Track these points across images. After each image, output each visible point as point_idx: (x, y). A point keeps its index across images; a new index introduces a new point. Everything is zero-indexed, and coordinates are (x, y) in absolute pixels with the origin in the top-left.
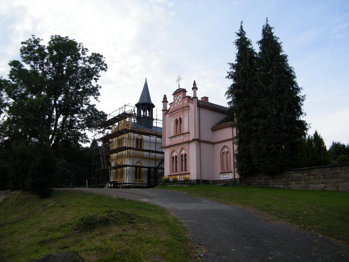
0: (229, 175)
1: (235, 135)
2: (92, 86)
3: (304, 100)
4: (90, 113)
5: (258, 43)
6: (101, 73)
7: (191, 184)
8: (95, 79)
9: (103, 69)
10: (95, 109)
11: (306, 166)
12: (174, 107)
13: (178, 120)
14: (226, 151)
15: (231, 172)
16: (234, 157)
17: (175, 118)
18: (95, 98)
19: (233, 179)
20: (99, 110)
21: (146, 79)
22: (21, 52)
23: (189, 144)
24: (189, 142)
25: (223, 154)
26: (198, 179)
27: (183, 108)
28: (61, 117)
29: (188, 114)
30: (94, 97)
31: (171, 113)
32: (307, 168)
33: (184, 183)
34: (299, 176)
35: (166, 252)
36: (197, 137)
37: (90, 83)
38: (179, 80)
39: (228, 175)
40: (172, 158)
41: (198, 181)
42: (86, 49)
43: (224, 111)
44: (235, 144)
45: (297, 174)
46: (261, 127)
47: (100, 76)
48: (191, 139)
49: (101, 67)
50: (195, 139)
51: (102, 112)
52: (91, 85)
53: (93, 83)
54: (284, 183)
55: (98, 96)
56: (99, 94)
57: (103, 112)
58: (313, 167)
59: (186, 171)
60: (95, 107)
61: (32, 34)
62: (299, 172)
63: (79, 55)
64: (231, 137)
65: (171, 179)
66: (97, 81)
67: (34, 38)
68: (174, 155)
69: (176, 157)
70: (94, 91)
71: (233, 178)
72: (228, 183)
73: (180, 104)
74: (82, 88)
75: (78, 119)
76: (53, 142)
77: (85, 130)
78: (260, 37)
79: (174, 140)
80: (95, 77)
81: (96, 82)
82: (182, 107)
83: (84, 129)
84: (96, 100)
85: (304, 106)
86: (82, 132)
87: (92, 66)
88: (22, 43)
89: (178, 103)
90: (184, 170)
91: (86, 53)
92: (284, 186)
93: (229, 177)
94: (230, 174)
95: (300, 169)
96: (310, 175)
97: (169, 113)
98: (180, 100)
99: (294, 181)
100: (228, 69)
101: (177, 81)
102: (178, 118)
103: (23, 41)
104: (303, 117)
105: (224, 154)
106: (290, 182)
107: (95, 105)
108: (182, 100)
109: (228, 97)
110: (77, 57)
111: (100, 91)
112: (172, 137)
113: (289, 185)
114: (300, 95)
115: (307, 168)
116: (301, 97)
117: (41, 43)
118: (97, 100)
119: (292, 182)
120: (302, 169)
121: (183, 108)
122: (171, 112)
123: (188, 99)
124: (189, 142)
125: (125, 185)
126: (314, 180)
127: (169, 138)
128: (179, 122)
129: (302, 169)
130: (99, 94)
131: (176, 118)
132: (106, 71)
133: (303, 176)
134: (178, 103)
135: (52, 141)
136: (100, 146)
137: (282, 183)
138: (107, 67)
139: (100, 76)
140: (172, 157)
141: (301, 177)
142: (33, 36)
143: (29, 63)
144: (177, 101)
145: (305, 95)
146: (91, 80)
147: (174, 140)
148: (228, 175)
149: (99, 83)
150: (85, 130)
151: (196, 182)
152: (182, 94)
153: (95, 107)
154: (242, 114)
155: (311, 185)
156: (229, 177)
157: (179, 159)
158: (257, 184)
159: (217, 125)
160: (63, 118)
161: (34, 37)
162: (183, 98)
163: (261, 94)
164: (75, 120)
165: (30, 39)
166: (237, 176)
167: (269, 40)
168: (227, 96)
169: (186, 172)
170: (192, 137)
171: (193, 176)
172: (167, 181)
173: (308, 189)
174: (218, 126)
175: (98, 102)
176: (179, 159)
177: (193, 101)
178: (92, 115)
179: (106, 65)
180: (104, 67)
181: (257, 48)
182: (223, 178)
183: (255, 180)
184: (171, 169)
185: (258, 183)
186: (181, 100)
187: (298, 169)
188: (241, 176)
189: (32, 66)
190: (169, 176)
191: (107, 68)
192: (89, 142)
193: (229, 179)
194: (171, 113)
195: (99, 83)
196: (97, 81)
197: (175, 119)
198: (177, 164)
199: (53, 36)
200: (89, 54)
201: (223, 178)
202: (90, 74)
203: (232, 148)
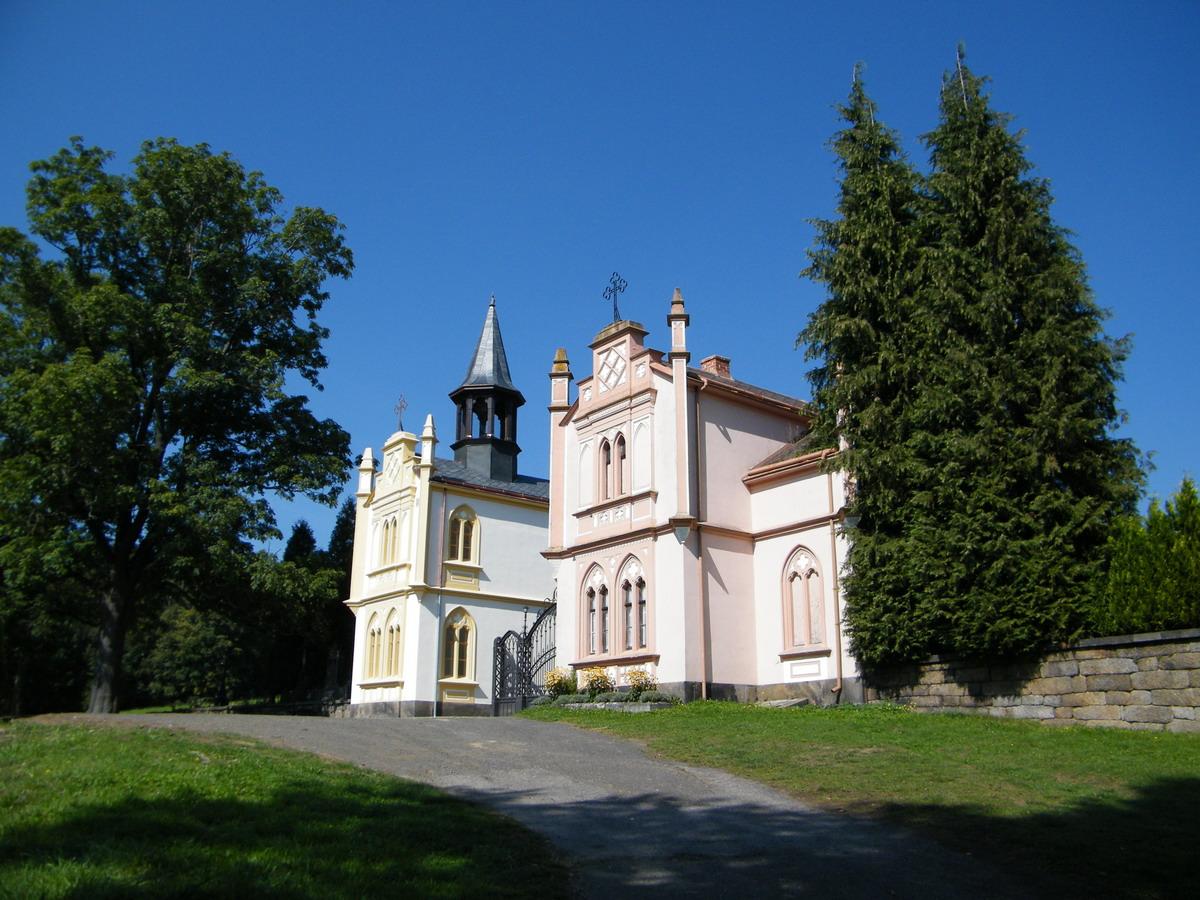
0: (794, 673)
1: (840, 503)
2: (295, 328)
3: (1126, 355)
4: (286, 427)
5: (926, 140)
6: (329, 284)
7: (666, 700)
8: (309, 306)
9: (336, 269)
10: (307, 412)
11: (1153, 629)
12: (597, 395)
13: (611, 444)
14: (803, 567)
15: (827, 653)
16: (836, 589)
17: (600, 437)
18: (309, 375)
19: (835, 680)
20: (320, 417)
21: (321, 388)
22: (31, 198)
23: (655, 540)
24: (654, 532)
25: (792, 580)
26: (692, 680)
27: (631, 398)
28: (178, 440)
29: (652, 421)
30: (304, 369)
31: (586, 416)
32: (1157, 636)
33: (636, 699)
34: (1124, 671)
35: (957, 239)
36: (686, 513)
37: (290, 316)
38: (615, 289)
39: (796, 676)
40: (585, 597)
41: (691, 689)
42: (275, 192)
43: (794, 410)
44: (843, 538)
45: (1115, 660)
46: (952, 464)
47: (326, 296)
48: (662, 520)
49: (329, 261)
50: (678, 517)
51: (330, 425)
52: (292, 325)
53: (301, 318)
54: (1056, 700)
55: (318, 369)
56: (321, 361)
57: (337, 427)
58: (1186, 634)
59: (645, 646)
60: (306, 406)
61: (73, 135)
62: (1121, 652)
63: (248, 215)
64: (825, 512)
65: (583, 680)
66: (317, 312)
67: (80, 148)
68: (593, 582)
69: (604, 591)
70: (305, 351)
71: (835, 675)
72: (815, 698)
73: (619, 379)
74: (259, 337)
75: (242, 449)
76: (144, 533)
77: (264, 490)
78: (934, 121)
79: (595, 525)
80: (307, 297)
81: (312, 316)
82: (627, 394)
83: (261, 488)
84: (308, 382)
85: (1123, 380)
86: (254, 498)
87: (297, 257)
88: (35, 168)
89: (613, 378)
90: (633, 642)
91: (274, 205)
92: (1055, 714)
93: (819, 674)
94: (823, 660)
95: (1126, 639)
96: (1171, 667)
97: (575, 417)
98: (620, 365)
99: (1101, 691)
100: (811, 243)
101: (607, 294)
102: (611, 436)
103: (39, 158)
104: (1117, 426)
105: (797, 578)
106: (1080, 695)
107: (304, 399)
108: (628, 366)
109: (814, 351)
110: (237, 223)
111: (326, 347)
112: (589, 512)
113: (1075, 710)
114: (1106, 338)
115: (1157, 636)
116: (1110, 346)
117: (109, 169)
118: (314, 382)
119: (1090, 697)
120: (1137, 638)
121: (631, 398)
122: (583, 413)
123: (651, 362)
124: (654, 532)
125: (253, 702)
126: (1190, 687)
127: (579, 515)
128: (615, 451)
129: (1137, 638)
130: (321, 361)
131: (605, 438)
132: (346, 274)
133: (1140, 670)
134: (613, 378)
135: (141, 530)
136: (321, 551)
137: (1047, 697)
138: (353, 261)
139: (326, 296)
140: (587, 589)
141: (1131, 673)
142: (73, 140)
143: (60, 238)
144: (608, 370)
145: (1130, 337)
146: (294, 307)
147: (595, 525)
148: (796, 676)
149: (322, 318)
150: (264, 490)
151: (682, 695)
152: (628, 342)
153: (306, 406)
154: (867, 418)
155: (1178, 711)
156: (819, 674)
157: (615, 600)
158: (937, 701)
159: (765, 465)
160: (185, 444)
161: (80, 142)
162: (632, 359)
163: (949, 331)
164: (228, 453)
165: (65, 152)
166: (850, 669)
167: (969, 129)
168: (805, 347)
169: (642, 652)
170: (662, 512)
171: (670, 672)
172: (563, 688)
173: (1164, 728)
174: (771, 466)
175: (315, 389)
176: (615, 600)
177: (671, 367)
178: (291, 432)
179: (347, 254)
180: (343, 261)
181: (918, 160)
182: (793, 676)
183: (929, 685)
184: (498, 603)
185: (941, 696)
186: (625, 366)
187: (1115, 640)
188: (867, 671)
189: (69, 250)
190: (577, 666)
191: (351, 264)
192: (280, 536)
193: (818, 683)
194: (586, 416)
195: (322, 318)
196: (317, 312)
197: (599, 441)
198: (607, 618)
199: (151, 145)
200: (284, 212)
201: (793, 676)
202: (287, 289)
203: (831, 551)
